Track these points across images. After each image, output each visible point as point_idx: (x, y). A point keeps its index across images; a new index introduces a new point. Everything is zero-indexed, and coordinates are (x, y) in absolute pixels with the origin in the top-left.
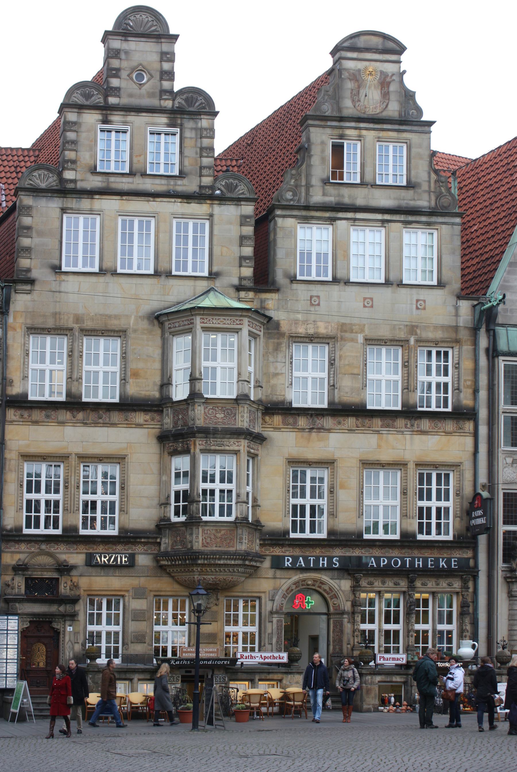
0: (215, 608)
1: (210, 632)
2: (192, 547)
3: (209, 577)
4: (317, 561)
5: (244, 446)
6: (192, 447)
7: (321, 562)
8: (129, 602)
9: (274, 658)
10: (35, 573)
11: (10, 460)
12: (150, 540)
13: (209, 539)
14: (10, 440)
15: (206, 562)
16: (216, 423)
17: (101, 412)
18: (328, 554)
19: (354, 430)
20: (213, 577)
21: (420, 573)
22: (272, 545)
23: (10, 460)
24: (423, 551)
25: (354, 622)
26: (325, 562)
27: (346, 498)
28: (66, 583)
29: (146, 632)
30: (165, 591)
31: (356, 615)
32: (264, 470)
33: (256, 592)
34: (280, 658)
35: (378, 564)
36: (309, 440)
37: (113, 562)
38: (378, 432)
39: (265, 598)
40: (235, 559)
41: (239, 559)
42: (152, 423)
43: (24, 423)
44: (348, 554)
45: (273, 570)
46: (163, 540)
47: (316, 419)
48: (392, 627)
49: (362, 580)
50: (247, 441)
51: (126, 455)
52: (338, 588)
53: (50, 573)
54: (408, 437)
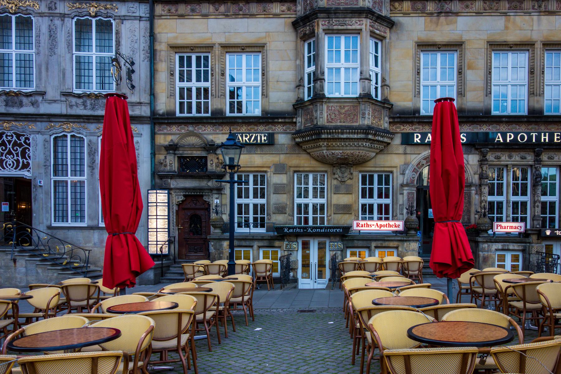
0: (349, 182)
1: (345, 203)
2: (317, 123)
3: (337, 151)
5: (366, 25)
6: (316, 28)
7: (543, 138)
8: (270, 177)
9: (390, 226)
10: (186, 152)
11: (160, 51)
12: (287, 120)
13: (334, 115)
14: (159, 33)
15: (329, 136)
16: (339, 4)
17: (241, 5)
19: (482, 13)
20: (341, 152)
21: (546, 147)
22: (403, 123)
23: (160, 51)
24: (549, 127)
25: (481, 194)
26: (547, 138)
27: (474, 78)
28: (212, 160)
29: (287, 204)
30: (303, 167)
31: (483, 187)
32: (394, 53)
33: (381, 167)
34: (395, 226)
35: (504, 138)
36: (437, 24)
37: (253, 141)
38: (505, 14)
39: (397, 172)
40: (358, 133)
41: (360, 133)
42: (289, 13)
43: (171, 17)
44: (475, 131)
45: (404, 146)
46: (298, 119)
47: (444, 4)
48: (520, 198)
49: (489, 154)
50: (369, 21)
51: (266, 44)
53: (199, 152)
54: (535, 18)
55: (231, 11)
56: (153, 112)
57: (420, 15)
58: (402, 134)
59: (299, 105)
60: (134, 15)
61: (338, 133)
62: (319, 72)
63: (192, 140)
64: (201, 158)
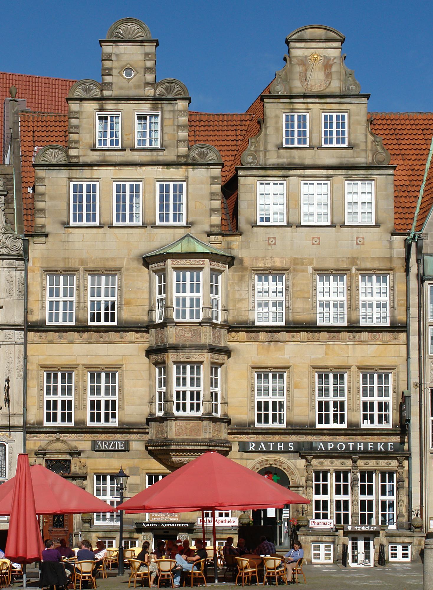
2: (167, 437)
4: (275, 445)
7: (279, 446)
9: (227, 522)
16: (185, 341)
18: (285, 440)
23: (32, 371)
26: (282, 447)
28: (76, 463)
32: (231, 375)
35: (326, 448)
38: (325, 343)
40: (201, 445)
42: (142, 340)
51: (122, 365)
52: (294, 467)
55: (93, 338)
56: (25, 423)
57: (254, 343)
58: (239, 442)
59: (151, 420)
60: (10, 340)
61: (185, 445)
62: (169, 395)
63: (58, 446)
64: (65, 461)
